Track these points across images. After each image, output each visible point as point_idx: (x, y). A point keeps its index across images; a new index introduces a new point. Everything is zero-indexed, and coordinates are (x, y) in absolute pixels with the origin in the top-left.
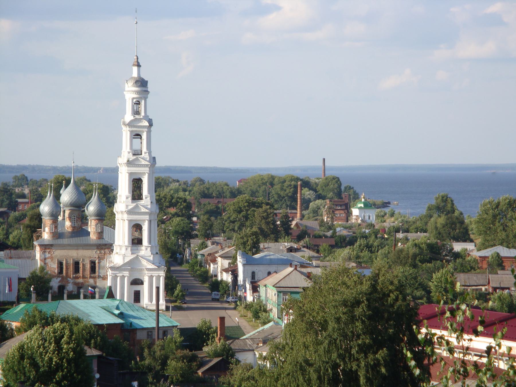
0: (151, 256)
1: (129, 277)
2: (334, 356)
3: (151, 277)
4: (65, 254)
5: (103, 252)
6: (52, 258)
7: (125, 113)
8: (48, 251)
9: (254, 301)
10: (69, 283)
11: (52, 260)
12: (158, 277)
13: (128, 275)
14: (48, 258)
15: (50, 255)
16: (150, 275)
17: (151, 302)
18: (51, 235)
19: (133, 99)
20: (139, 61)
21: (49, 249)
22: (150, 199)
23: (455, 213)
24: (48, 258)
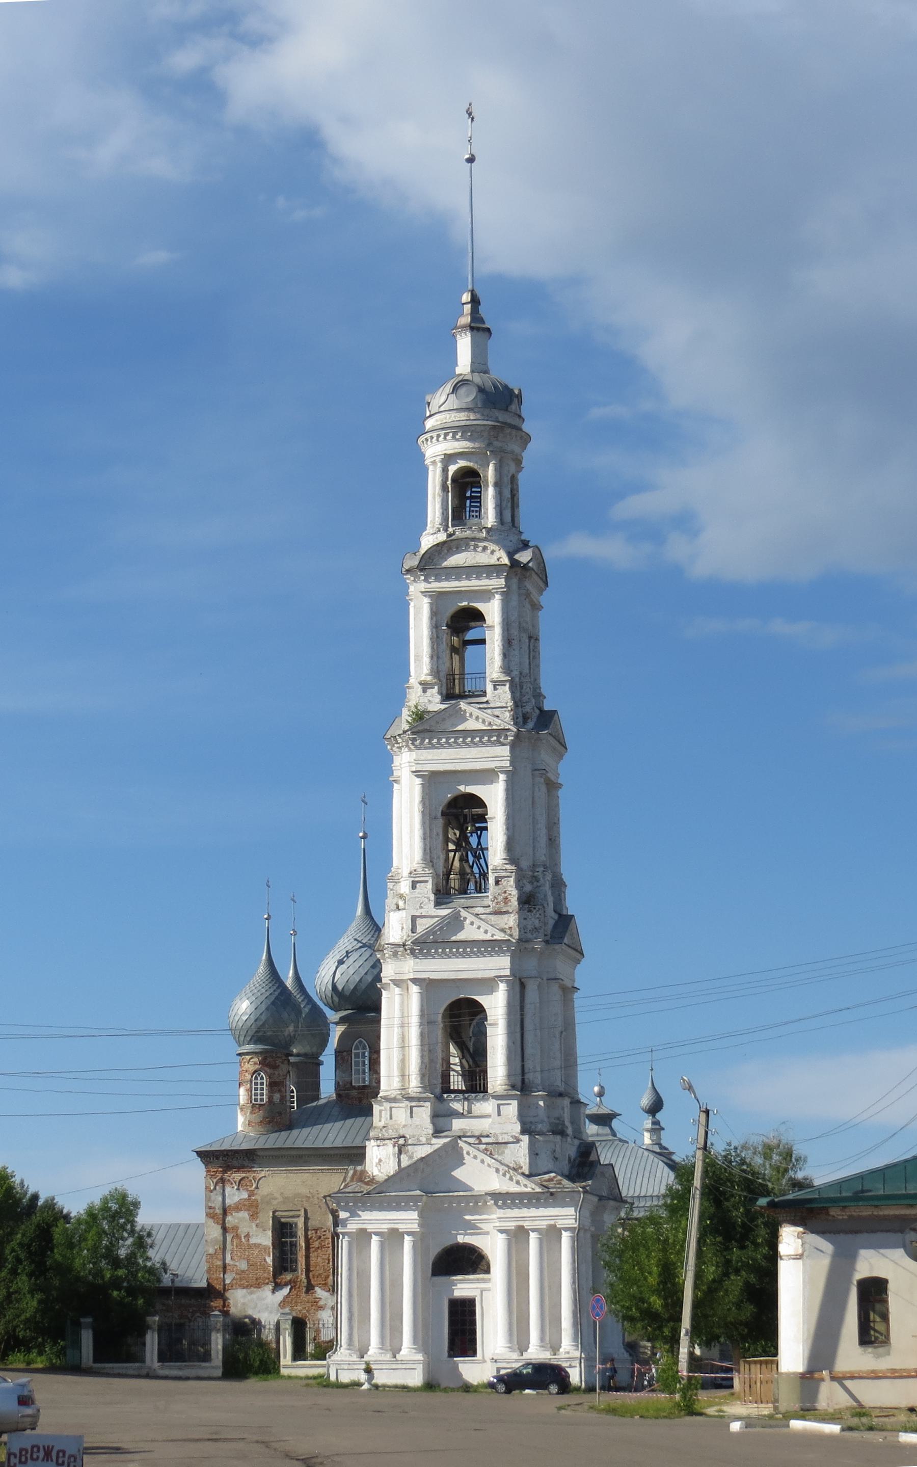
0: (518, 1141)
1: (421, 1241)
2: (663, 1214)
3: (517, 1237)
4: (304, 1191)
5: (704, 1288)
6: (252, 1207)
7: (422, 526)
8: (237, 1176)
9: (524, 703)
10: (321, 1308)
11: (254, 1216)
12: (551, 1234)
13: (415, 1227)
14: (238, 1207)
15: (245, 1195)
16: (511, 1225)
17: (396, 1351)
18: (259, 1116)
19: (449, 459)
20: (887, 1259)
21: (239, 1168)
22: (519, 885)
23: (910, 1426)
24: (238, 1207)
